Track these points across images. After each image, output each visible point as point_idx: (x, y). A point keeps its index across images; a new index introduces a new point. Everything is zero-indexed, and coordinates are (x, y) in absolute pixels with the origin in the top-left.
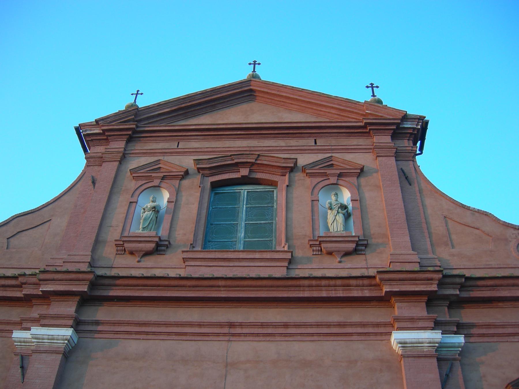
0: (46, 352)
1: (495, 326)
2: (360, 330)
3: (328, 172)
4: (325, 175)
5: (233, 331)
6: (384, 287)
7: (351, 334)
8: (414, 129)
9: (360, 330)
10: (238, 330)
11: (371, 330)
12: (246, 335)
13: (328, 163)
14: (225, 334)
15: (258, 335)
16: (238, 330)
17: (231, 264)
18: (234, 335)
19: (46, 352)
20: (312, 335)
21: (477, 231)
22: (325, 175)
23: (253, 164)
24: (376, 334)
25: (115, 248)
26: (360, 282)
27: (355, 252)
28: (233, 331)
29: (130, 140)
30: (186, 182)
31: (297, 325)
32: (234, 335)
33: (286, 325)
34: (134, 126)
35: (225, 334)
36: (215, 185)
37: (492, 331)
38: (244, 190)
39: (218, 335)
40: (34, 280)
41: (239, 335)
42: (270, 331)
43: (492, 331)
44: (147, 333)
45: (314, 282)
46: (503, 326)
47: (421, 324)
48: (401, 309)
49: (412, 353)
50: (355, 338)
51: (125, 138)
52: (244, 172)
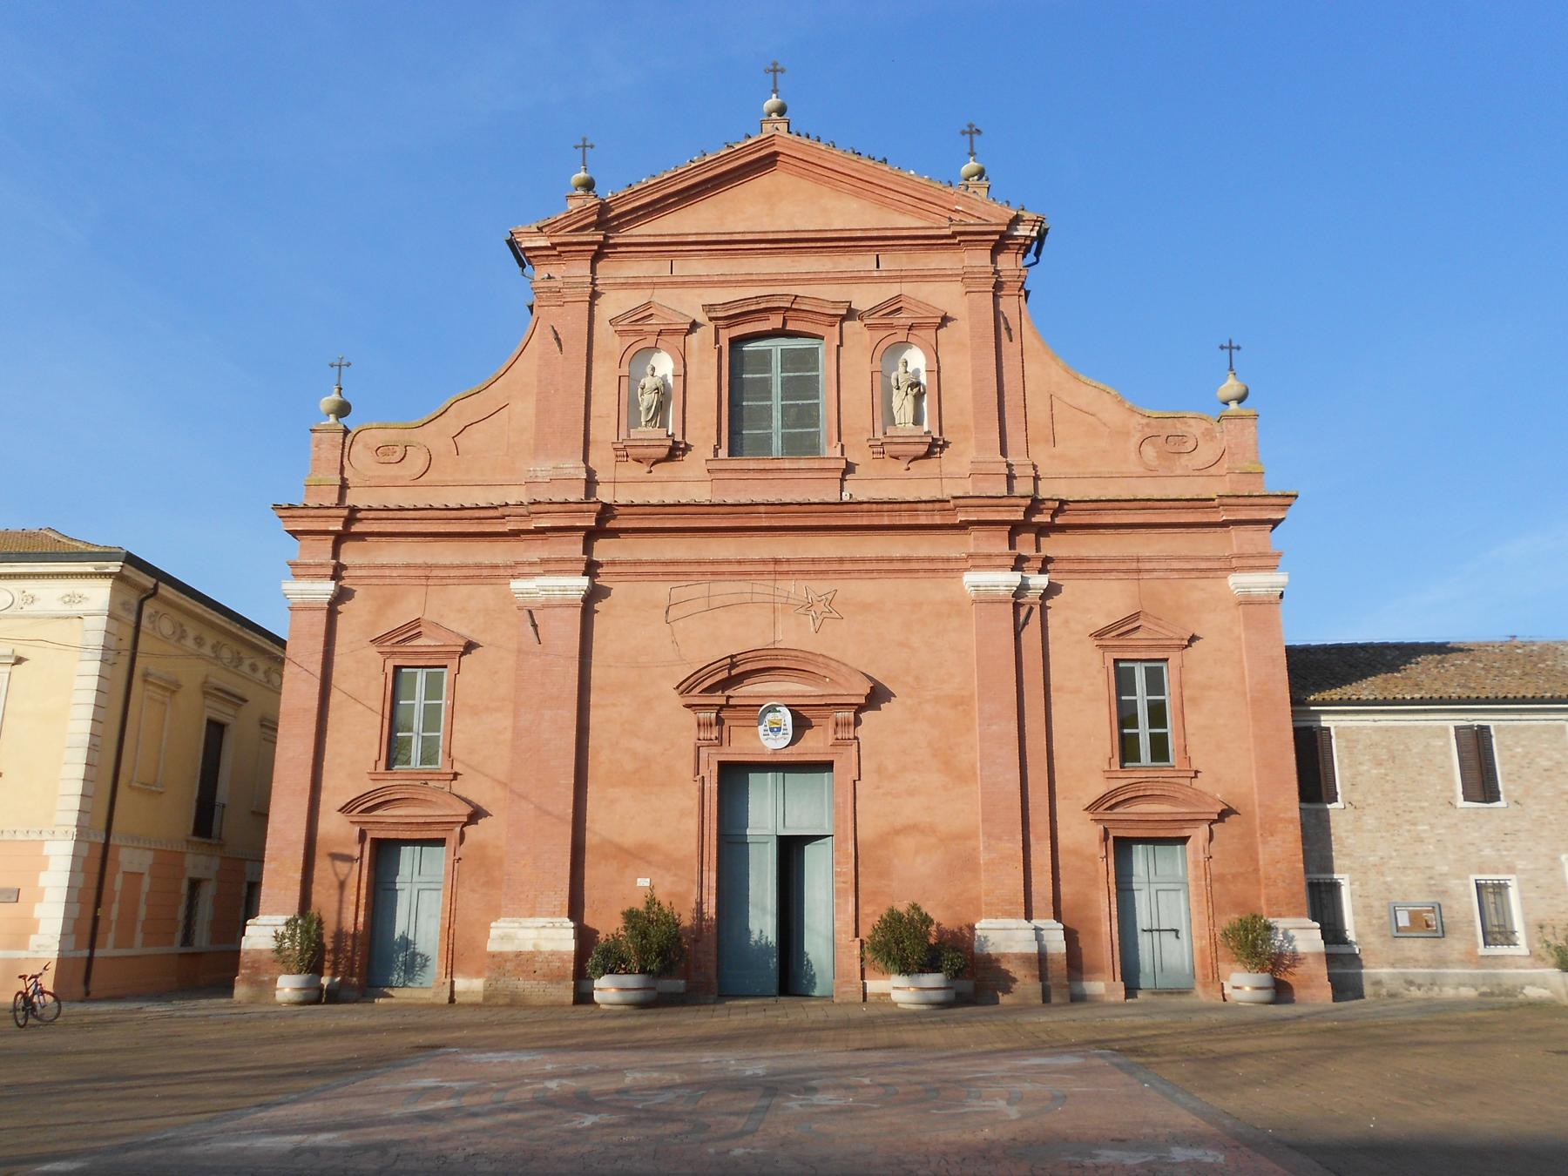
0: (560, 606)
1: (1089, 560)
2: (927, 566)
3: (895, 322)
4: (891, 326)
5: (779, 568)
6: (598, 983)
7: (917, 571)
8: (1026, 237)
9: (927, 566)
10: (785, 568)
11: (940, 565)
12: (794, 572)
13: (894, 307)
14: (769, 573)
15: (808, 572)
16: (785, 568)
17: (770, 476)
18: (781, 573)
19: (560, 606)
20: (872, 571)
21: (1091, 419)
22: (891, 326)
23: (788, 309)
24: (946, 570)
25: (613, 454)
26: (930, 506)
27: (928, 455)
28: (779, 568)
29: (597, 257)
30: (694, 339)
31: (853, 560)
32: (781, 573)
33: (841, 560)
34: (600, 238)
35: (769, 573)
36: (736, 342)
37: (1084, 566)
38: (777, 346)
39: (762, 573)
40: (522, 511)
41: (787, 573)
42: (823, 567)
43: (1084, 566)
44: (677, 574)
45: (874, 507)
46: (1100, 561)
47: (998, 561)
48: (972, 542)
49: (985, 600)
50: (921, 574)
51: (589, 256)
52: (775, 322)
